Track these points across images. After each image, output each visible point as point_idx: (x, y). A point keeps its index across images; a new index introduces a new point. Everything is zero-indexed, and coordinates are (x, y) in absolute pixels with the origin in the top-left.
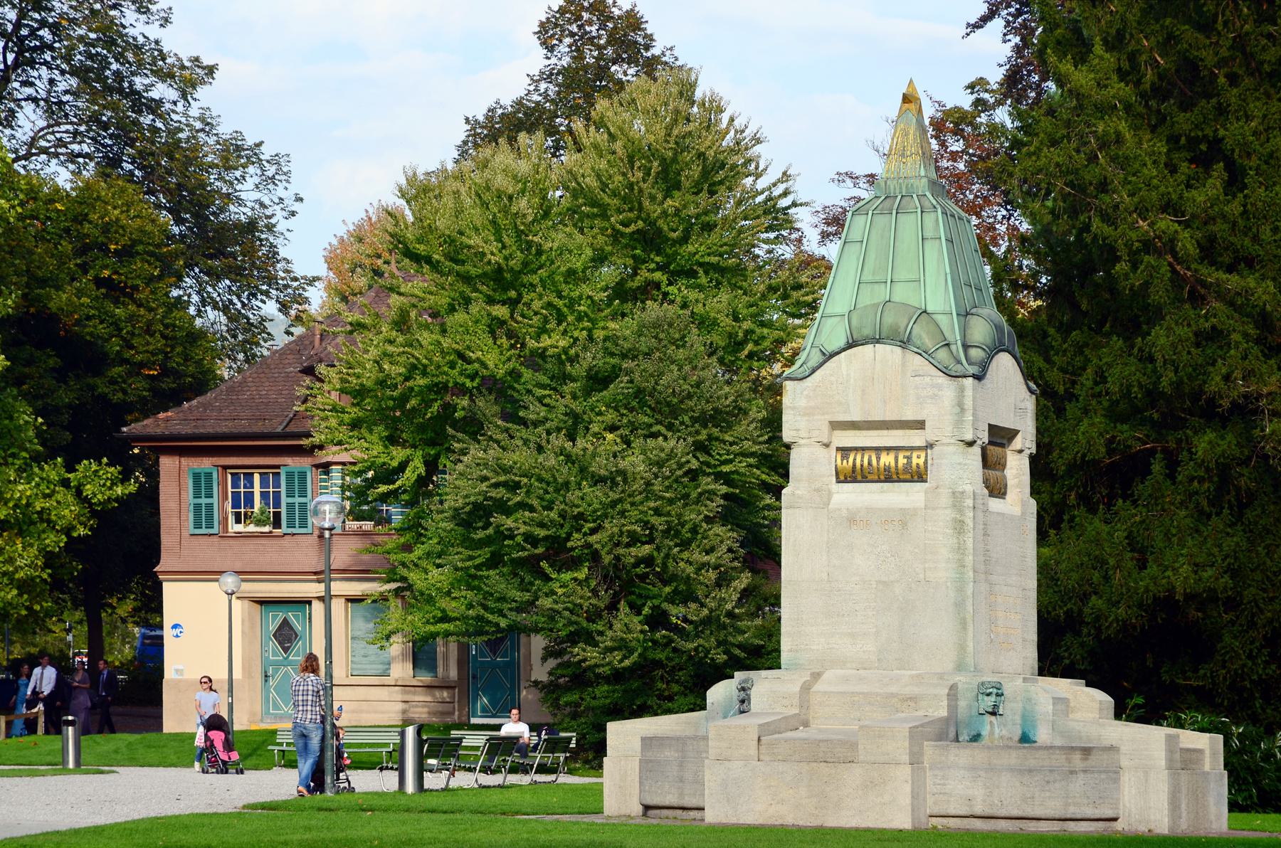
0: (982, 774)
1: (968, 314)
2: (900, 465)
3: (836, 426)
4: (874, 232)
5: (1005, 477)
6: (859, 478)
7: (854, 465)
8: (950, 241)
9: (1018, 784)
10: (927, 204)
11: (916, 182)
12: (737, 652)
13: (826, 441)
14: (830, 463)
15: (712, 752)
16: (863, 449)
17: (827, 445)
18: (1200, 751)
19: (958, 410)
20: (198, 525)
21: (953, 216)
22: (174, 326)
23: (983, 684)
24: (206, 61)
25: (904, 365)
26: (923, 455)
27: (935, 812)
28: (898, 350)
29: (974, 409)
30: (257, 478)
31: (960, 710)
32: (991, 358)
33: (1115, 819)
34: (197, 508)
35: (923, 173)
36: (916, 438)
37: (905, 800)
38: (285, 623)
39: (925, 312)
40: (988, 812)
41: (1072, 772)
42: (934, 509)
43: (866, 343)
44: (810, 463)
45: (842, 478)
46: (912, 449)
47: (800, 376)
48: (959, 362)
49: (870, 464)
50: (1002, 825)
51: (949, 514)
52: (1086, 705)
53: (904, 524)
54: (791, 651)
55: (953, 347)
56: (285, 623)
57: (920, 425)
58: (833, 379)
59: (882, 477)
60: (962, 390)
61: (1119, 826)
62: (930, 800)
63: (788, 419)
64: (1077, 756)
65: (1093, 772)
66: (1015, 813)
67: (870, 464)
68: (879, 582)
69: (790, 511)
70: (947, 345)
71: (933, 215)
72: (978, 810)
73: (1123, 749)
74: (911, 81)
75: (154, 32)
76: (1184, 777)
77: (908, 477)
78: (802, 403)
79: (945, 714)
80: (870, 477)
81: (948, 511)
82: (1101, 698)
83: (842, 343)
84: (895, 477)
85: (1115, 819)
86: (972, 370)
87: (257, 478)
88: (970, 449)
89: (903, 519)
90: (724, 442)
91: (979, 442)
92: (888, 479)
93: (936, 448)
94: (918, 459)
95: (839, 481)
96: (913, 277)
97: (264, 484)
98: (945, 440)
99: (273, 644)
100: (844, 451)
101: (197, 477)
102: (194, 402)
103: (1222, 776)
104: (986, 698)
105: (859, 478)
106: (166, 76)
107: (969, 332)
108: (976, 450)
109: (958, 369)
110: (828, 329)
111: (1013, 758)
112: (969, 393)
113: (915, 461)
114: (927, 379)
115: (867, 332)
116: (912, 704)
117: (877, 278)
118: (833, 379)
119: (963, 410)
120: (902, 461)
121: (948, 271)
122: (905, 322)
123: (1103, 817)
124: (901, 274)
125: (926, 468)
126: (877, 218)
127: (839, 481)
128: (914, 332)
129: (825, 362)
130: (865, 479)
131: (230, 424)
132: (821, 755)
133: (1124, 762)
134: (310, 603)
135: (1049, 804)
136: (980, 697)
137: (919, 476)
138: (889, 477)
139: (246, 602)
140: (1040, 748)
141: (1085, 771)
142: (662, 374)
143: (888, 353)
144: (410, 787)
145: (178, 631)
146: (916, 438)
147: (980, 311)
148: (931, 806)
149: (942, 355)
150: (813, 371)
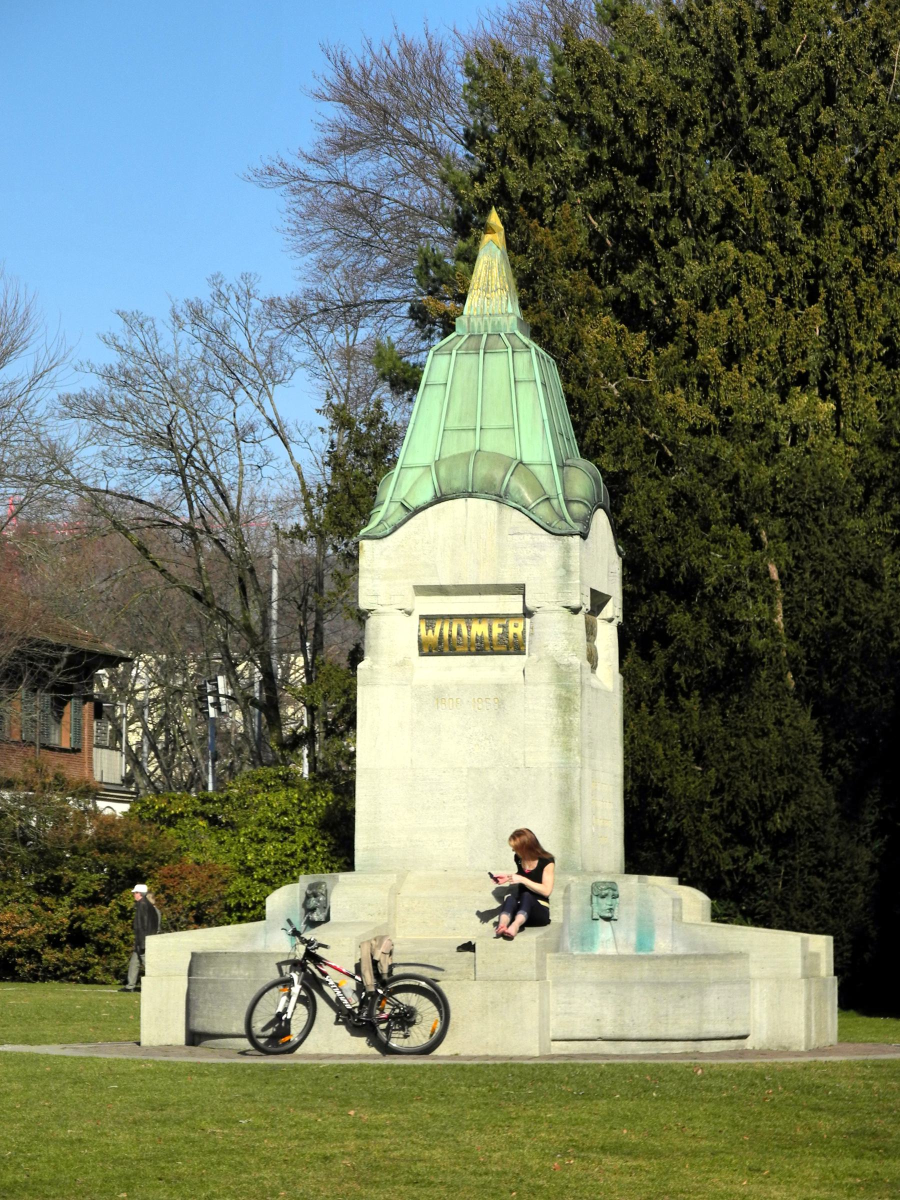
3: (423, 590)
4: (458, 375)
6: (446, 650)
7: (441, 635)
8: (544, 385)
11: (503, 320)
13: (408, 608)
16: (451, 617)
17: (409, 613)
19: (562, 572)
25: (500, 522)
26: (521, 624)
27: (558, 1037)
28: (494, 505)
29: (581, 571)
32: (592, 513)
33: (744, 1037)
36: (513, 605)
37: (532, 1023)
39: (521, 462)
40: (618, 1034)
43: (457, 497)
44: (391, 639)
45: (426, 650)
47: (381, 534)
48: (562, 518)
49: (459, 634)
50: (677, 1047)
52: (675, 905)
54: (366, 849)
55: (555, 502)
57: (520, 589)
59: (473, 649)
60: (567, 549)
61: (749, 1044)
62: (553, 1023)
66: (646, 1034)
67: (459, 634)
72: (608, 1032)
73: (753, 956)
77: (504, 648)
80: (459, 649)
82: (695, 901)
83: (428, 496)
84: (488, 649)
85: (744, 1037)
86: (578, 527)
88: (575, 617)
91: (584, 609)
94: (515, 629)
95: (422, 654)
100: (429, 620)
103: (830, 983)
104: (601, 900)
105: (446, 650)
108: (581, 617)
112: (576, 553)
113: (512, 630)
114: (528, 538)
115: (458, 484)
117: (465, 425)
119: (568, 572)
120: (497, 631)
121: (546, 418)
122: (501, 474)
123: (737, 1034)
124: (492, 421)
125: (524, 638)
126: (461, 358)
127: (422, 654)
129: (408, 518)
133: (754, 971)
135: (683, 1023)
136: (595, 899)
137: (516, 647)
138: (481, 648)
143: (482, 509)
146: (513, 605)
148: (556, 1028)
149: (543, 511)
150: (395, 528)
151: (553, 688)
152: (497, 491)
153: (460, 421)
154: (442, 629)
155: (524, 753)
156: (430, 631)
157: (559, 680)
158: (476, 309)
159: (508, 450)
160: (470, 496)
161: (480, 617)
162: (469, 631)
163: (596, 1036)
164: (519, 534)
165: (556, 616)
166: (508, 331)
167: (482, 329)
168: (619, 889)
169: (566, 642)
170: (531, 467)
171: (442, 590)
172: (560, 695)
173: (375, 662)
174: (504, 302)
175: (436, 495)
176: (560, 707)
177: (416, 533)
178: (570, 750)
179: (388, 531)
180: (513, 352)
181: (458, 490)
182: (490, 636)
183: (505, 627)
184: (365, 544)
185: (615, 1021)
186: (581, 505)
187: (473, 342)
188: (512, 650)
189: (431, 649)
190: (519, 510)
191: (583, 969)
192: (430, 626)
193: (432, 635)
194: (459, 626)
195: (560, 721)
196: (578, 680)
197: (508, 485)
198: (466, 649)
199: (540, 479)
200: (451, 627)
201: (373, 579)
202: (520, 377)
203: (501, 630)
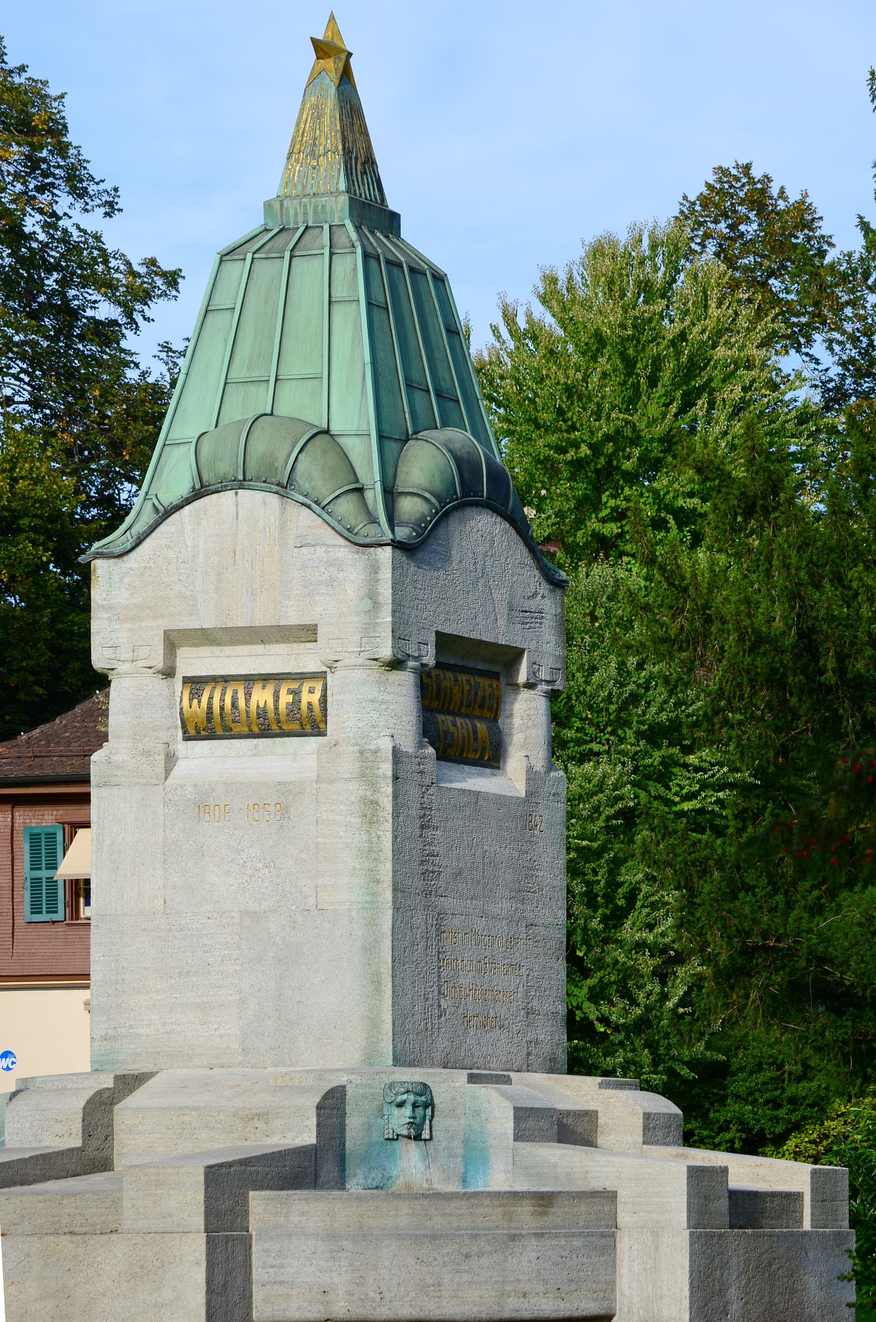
0: (347, 1244)
9: (411, 1261)
12: (685, 1072)
14: (171, 706)
16: (226, 679)
18: (796, 1197)
19: (367, 604)
20: (36, 909)
22: (71, 633)
23: (391, 1086)
24: (167, 265)
25: (283, 526)
28: (273, 500)
31: (349, 1135)
34: (36, 883)
35: (342, 186)
39: (327, 432)
41: (513, 1238)
42: (331, 782)
45: (192, 732)
46: (302, 677)
47: (118, 550)
49: (234, 705)
51: (355, 790)
53: (284, 811)
55: (369, 495)
57: (308, 633)
58: (171, 554)
59: (256, 729)
60: (374, 569)
64: (526, 1209)
65: (557, 1236)
67: (234, 705)
68: (245, 913)
69: (104, 791)
71: (349, 259)
74: (332, 18)
75: (94, 221)
76: (738, 1243)
77: (295, 726)
78: (122, 598)
79: (313, 1141)
81: (353, 786)
83: (183, 489)
89: (280, 803)
90: (686, 766)
92: (265, 733)
94: (310, 697)
95: (187, 738)
96: (311, 371)
101: (35, 839)
102: (36, 732)
104: (396, 1111)
105: (219, 731)
106: (107, 286)
109: (370, 533)
110: (171, 471)
113: (305, 698)
114: (320, 551)
115: (225, 467)
116: (260, 1125)
117: (256, 374)
118: (171, 554)
119: (376, 605)
120: (285, 699)
124: (292, 367)
128: (301, 468)
130: (228, 734)
132: (65, 1221)
137: (312, 725)
138: (265, 727)
140: (398, 1196)
141: (540, 1236)
142: (594, 669)
143: (258, 503)
145: (9, 1061)
149: (346, 507)
153: (250, 367)
154: (211, 698)
156: (195, 701)
161: (265, 678)
162: (247, 701)
164: (308, 545)
165: (359, 675)
166: (337, 222)
167: (300, 219)
170: (341, 441)
174: (335, 174)
175: (194, 488)
180: (331, 254)
182: (276, 708)
183: (296, 693)
184: (100, 567)
186: (418, 500)
188: (308, 728)
190: (309, 507)
192: (195, 695)
193: (199, 709)
194: (235, 692)
195: (365, 837)
198: (246, 730)
199: (353, 458)
200: (223, 694)
203: (290, 698)
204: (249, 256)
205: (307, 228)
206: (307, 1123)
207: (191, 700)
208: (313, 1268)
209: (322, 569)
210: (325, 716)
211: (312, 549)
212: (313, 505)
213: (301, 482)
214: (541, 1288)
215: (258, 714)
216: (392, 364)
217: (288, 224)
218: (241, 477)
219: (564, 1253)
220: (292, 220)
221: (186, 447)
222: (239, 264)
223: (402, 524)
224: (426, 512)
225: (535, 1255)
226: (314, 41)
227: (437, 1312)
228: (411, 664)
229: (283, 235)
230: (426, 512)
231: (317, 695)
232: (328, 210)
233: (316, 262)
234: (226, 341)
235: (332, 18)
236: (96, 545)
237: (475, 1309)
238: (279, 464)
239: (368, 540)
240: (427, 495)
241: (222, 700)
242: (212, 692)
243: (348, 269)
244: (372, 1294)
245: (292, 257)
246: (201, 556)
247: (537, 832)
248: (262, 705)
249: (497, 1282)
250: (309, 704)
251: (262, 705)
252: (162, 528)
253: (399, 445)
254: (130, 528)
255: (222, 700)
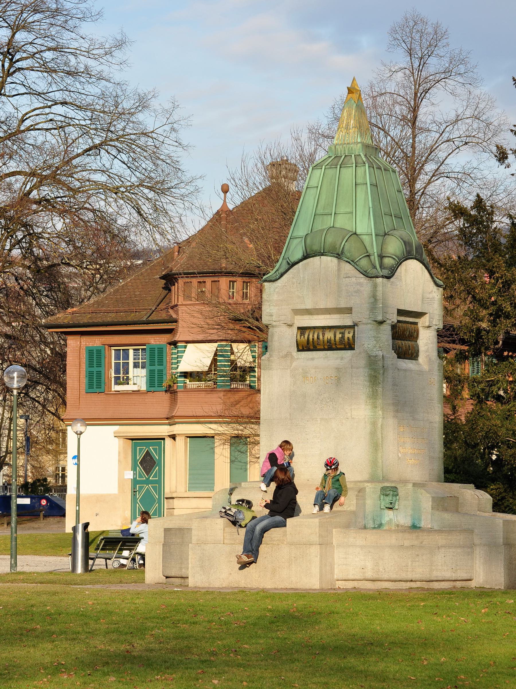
1: (385, 234)
2: (337, 338)
3: (297, 312)
5: (418, 346)
6: (312, 348)
10: (360, 161)
13: (289, 323)
15: (194, 539)
16: (315, 328)
17: (290, 326)
19: (372, 300)
21: (379, 168)
25: (339, 270)
28: (335, 260)
30: (131, 353)
32: (399, 264)
37: (315, 570)
38: (148, 454)
39: (355, 234)
40: (375, 576)
43: (315, 256)
45: (301, 348)
47: (274, 279)
48: (375, 267)
55: (372, 257)
56: (148, 454)
57: (349, 310)
60: (375, 286)
62: (336, 571)
63: (266, 309)
70: (368, 256)
71: (363, 168)
77: (342, 346)
78: (275, 297)
80: (318, 347)
82: (485, 498)
83: (299, 255)
86: (386, 272)
87: (131, 353)
92: (330, 349)
93: (360, 327)
94: (348, 335)
95: (299, 350)
96: (349, 210)
97: (117, 357)
98: (365, 321)
99: (139, 468)
100: (302, 330)
107: (384, 246)
109: (374, 272)
111: (409, 539)
113: (347, 335)
114: (354, 279)
117: (326, 211)
120: (339, 336)
124: (342, 209)
127: (299, 350)
128: (346, 248)
130: (315, 349)
131: (113, 315)
134: (164, 439)
136: (382, 497)
137: (349, 346)
138: (330, 347)
139: (122, 440)
144: (80, 569)
147: (395, 232)
149: (364, 263)
150: (282, 275)
151: (367, 370)
152: (337, 252)
153: (324, 209)
154: (309, 335)
155: (351, 409)
156: (303, 336)
157: (370, 365)
158: (341, 140)
159: (349, 227)
160: (322, 255)
161: (330, 328)
162: (323, 336)
163: (362, 578)
164: (349, 277)
166: (357, 154)
167: (343, 153)
168: (399, 491)
169: (375, 342)
170: (361, 237)
171: (308, 312)
172: (371, 374)
173: (271, 356)
174: (356, 136)
175: (304, 255)
176: (371, 381)
177: (293, 278)
178: (376, 407)
179: (278, 277)
180: (356, 166)
181: (316, 252)
182: (335, 339)
183: (343, 334)
185: (373, 569)
186: (390, 259)
187: (335, 161)
189: (304, 347)
190: (349, 263)
191: (354, 538)
192: (302, 334)
196: (381, 365)
197: (343, 248)
200: (313, 334)
201: (269, 305)
202: (359, 181)
204: (324, 167)
205: (345, 156)
206: (352, 502)
207: (301, 336)
208: (358, 559)
209: (354, 286)
210: (354, 342)
211: (350, 279)
212: (351, 262)
213: (346, 253)
214: (446, 568)
215: (328, 341)
216: (379, 207)
217: (338, 154)
218: (322, 252)
219: (455, 555)
220: (339, 153)
221: (299, 240)
222: (320, 170)
223: (384, 268)
224: (394, 263)
225: (443, 555)
226: (348, 88)
227: (406, 577)
228: (388, 322)
229: (336, 159)
230: (394, 263)
231: (351, 334)
232: (354, 149)
233: (350, 170)
234: (315, 199)
235: (354, 79)
236: (265, 277)
237: (421, 576)
238: (338, 246)
239: (373, 276)
240: (394, 257)
241: (313, 336)
242: (309, 333)
243: (363, 172)
244: (381, 570)
245: (340, 167)
246: (306, 281)
247: (432, 385)
248: (329, 338)
249: (429, 566)
250: (348, 338)
251: (329, 338)
252: (291, 270)
253: (382, 237)
254: (277, 270)
255: (313, 336)
